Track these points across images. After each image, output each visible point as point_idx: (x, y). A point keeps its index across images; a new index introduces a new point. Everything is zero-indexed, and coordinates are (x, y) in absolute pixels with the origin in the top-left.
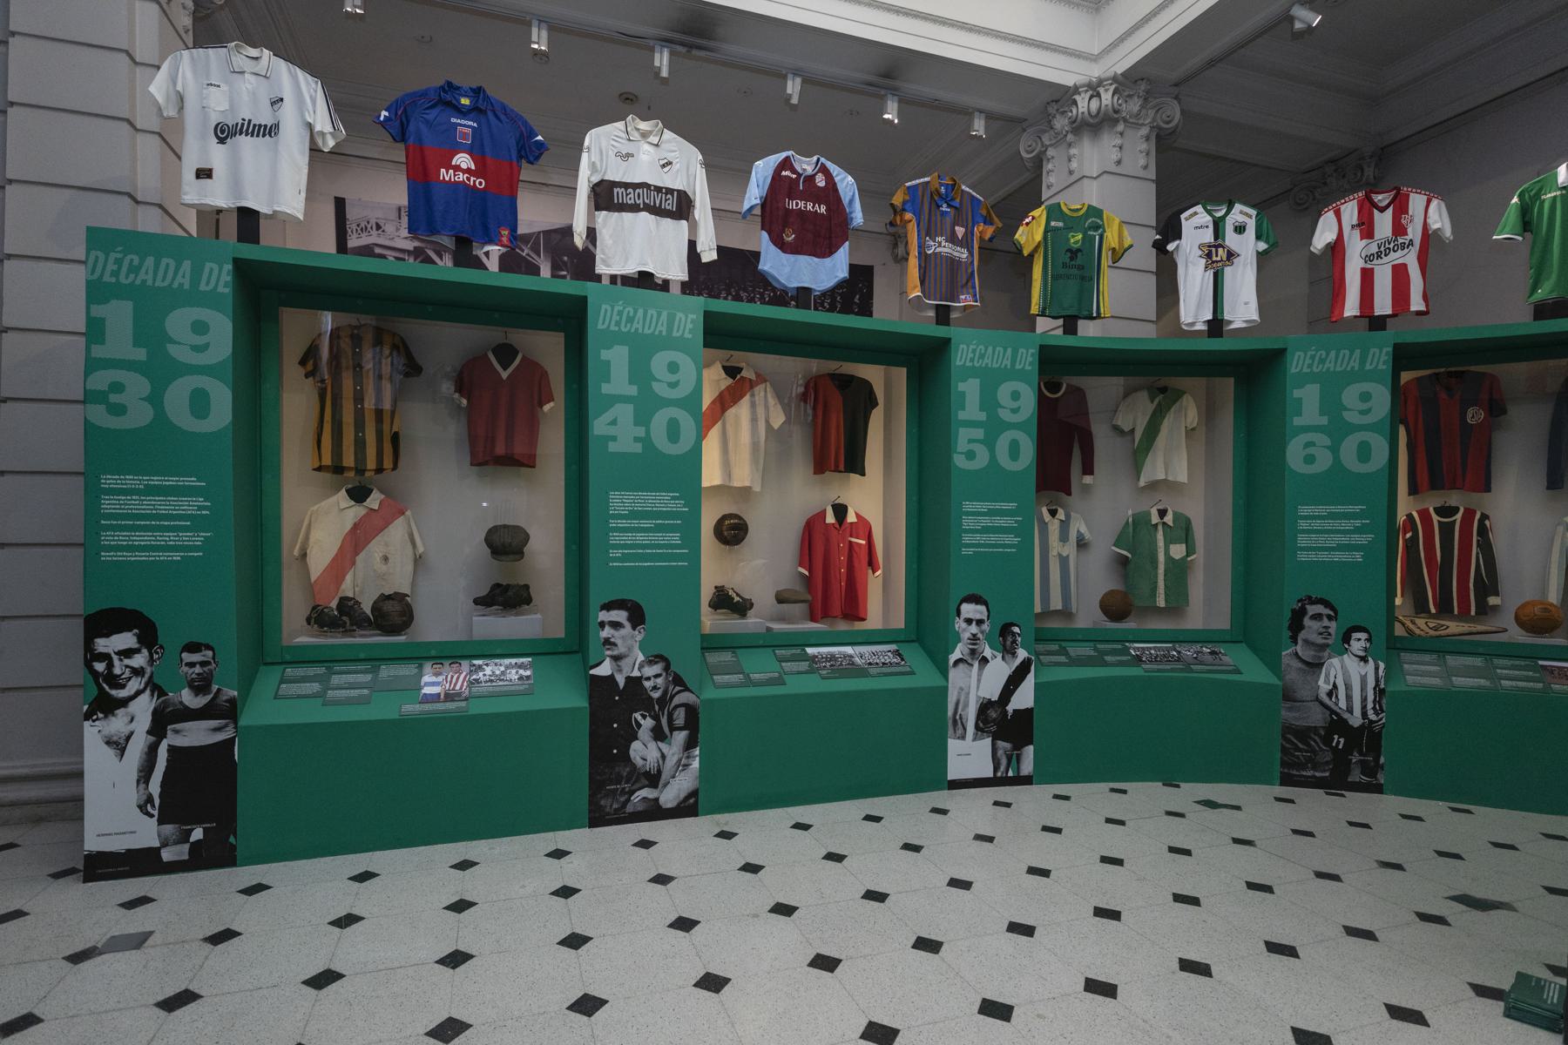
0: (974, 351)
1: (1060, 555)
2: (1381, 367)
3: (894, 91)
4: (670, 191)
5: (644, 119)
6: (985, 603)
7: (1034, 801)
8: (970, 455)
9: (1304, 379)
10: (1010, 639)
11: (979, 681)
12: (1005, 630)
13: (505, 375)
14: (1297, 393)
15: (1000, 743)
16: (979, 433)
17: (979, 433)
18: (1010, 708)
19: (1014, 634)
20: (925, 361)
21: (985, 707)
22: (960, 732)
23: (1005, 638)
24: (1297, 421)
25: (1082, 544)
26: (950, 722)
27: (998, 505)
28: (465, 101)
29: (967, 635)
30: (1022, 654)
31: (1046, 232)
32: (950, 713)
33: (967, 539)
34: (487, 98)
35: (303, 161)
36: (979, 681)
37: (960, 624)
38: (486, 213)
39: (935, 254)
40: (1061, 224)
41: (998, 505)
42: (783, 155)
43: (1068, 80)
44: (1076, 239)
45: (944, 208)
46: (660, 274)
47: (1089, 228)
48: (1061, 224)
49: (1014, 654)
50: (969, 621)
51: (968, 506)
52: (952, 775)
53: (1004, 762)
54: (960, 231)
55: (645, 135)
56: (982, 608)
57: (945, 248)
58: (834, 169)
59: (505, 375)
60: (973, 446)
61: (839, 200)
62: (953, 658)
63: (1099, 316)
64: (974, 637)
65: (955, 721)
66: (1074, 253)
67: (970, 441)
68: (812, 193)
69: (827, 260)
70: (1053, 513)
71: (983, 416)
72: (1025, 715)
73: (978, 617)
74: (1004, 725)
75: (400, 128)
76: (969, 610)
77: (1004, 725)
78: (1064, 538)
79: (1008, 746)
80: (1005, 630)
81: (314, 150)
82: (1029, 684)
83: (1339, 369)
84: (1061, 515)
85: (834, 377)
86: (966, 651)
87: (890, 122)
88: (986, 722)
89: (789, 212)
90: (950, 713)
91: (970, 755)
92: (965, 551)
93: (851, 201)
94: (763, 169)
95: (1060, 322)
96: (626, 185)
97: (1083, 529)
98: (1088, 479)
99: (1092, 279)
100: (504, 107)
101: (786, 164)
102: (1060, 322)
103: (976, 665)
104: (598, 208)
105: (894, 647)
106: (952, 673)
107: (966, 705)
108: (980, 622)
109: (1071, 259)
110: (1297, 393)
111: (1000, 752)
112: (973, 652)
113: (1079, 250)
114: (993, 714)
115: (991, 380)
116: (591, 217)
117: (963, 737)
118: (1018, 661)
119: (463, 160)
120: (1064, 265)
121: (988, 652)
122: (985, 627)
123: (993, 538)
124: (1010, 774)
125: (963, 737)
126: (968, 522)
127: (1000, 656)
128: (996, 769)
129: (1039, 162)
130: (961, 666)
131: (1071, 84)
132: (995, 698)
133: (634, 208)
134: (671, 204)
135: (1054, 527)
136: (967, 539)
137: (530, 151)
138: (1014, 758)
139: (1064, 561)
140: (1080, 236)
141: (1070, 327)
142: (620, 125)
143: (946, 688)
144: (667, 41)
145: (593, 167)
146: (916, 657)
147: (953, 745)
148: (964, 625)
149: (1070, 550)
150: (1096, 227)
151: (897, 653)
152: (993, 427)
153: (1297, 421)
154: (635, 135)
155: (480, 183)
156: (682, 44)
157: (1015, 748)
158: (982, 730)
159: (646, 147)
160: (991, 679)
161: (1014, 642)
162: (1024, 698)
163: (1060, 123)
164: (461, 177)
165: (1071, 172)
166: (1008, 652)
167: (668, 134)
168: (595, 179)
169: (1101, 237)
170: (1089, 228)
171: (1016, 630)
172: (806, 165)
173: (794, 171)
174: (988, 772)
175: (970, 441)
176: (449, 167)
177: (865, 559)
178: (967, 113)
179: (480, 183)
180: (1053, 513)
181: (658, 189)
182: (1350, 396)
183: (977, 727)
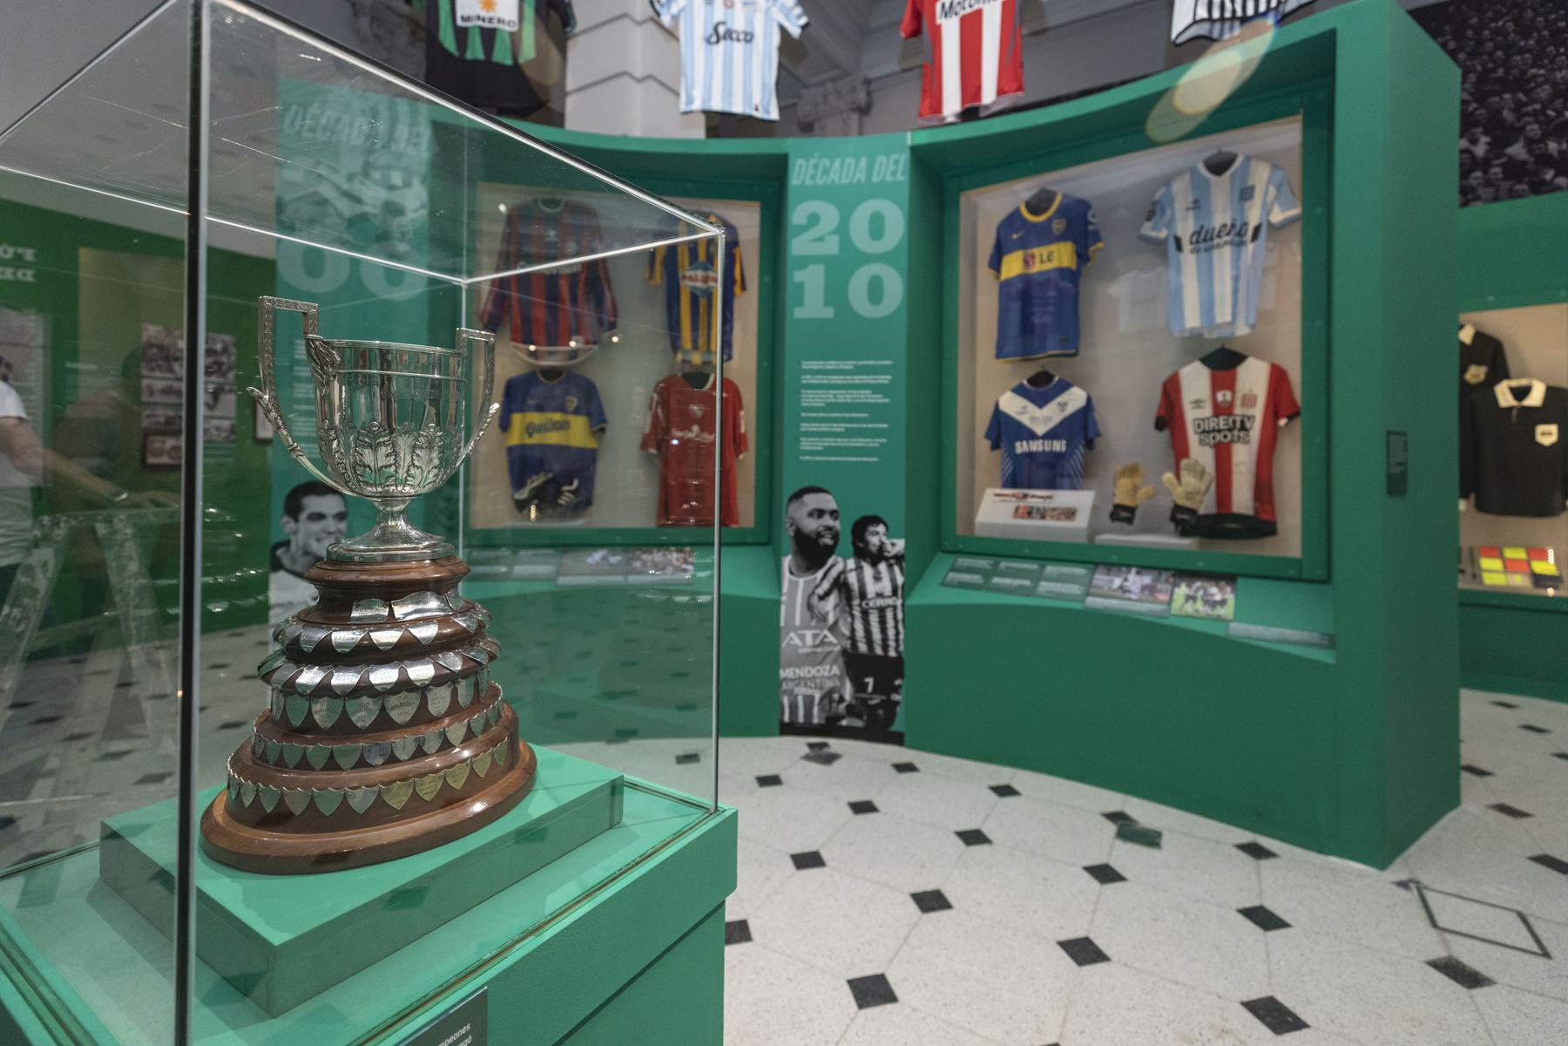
51: (806, 365)
83: (844, 181)
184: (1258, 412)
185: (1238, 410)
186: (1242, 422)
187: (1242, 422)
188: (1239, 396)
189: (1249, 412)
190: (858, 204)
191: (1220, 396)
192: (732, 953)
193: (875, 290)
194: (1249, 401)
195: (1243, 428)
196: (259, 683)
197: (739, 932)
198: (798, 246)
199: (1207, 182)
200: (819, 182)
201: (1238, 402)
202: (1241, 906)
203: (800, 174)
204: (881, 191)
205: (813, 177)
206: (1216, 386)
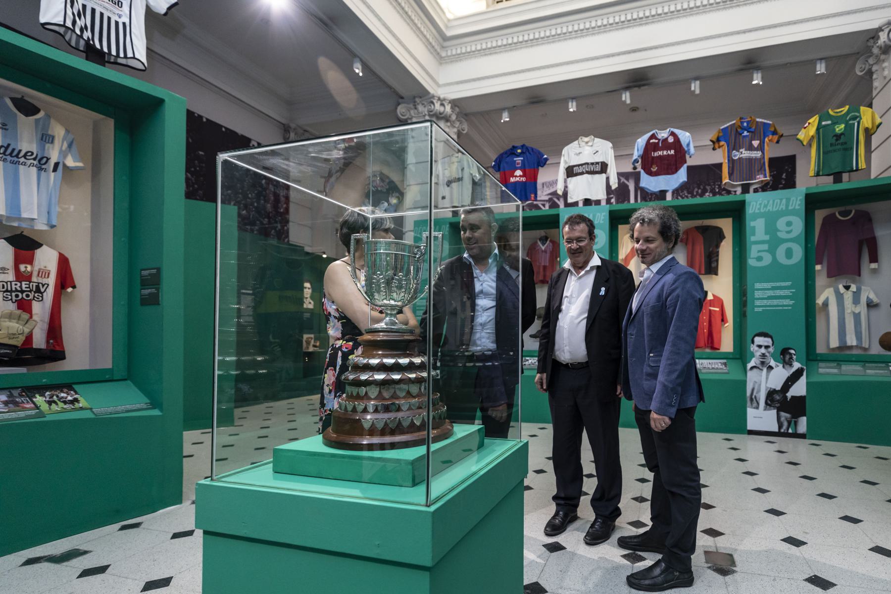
0: (760, 204)
1: (854, 313)
2: (797, 207)
3: (758, 68)
4: (597, 163)
5: (586, 136)
6: (771, 337)
7: (800, 449)
8: (759, 259)
9: (756, 217)
10: (788, 357)
11: (767, 378)
12: (785, 352)
13: (543, 248)
14: (752, 224)
15: (782, 414)
16: (765, 247)
17: (765, 247)
18: (789, 395)
19: (791, 354)
20: (737, 212)
21: (771, 394)
22: (755, 404)
23: (785, 356)
24: (753, 239)
25: (871, 305)
26: (748, 400)
27: (778, 284)
28: (519, 151)
29: (758, 354)
30: (797, 365)
31: (818, 129)
32: (748, 394)
33: (757, 303)
34: (527, 148)
35: (470, 187)
36: (767, 378)
37: (753, 348)
38: (526, 191)
39: (740, 159)
40: (829, 122)
41: (778, 284)
42: (651, 133)
43: (875, 25)
44: (840, 128)
45: (745, 133)
46: (594, 198)
47: (850, 119)
48: (829, 122)
49: (791, 365)
50: (760, 346)
51: (758, 286)
52: (750, 427)
53: (785, 424)
54: (756, 143)
55: (587, 143)
56: (769, 340)
57: (745, 154)
58: (676, 131)
59: (543, 248)
60: (760, 254)
61: (681, 145)
62: (749, 366)
63: (857, 170)
64: (763, 355)
65: (751, 400)
66: (838, 137)
67: (759, 251)
68: (665, 144)
69: (675, 176)
70: (847, 288)
71: (767, 238)
72: (799, 401)
73: (766, 344)
74: (777, 400)
75: (498, 167)
76: (759, 340)
77: (777, 400)
78: (856, 300)
79: (788, 415)
80: (785, 352)
81: (473, 181)
82: (802, 381)
83: (775, 209)
84: (854, 288)
85: (697, 228)
86: (758, 362)
87: (758, 84)
88: (773, 401)
89: (653, 158)
90: (748, 394)
91: (762, 418)
92: (756, 309)
93: (688, 145)
94: (641, 142)
95: (832, 177)
96: (579, 166)
97: (872, 296)
98: (874, 266)
99: (852, 149)
100: (532, 149)
101: (653, 136)
102: (832, 177)
103: (765, 370)
104: (568, 177)
105: (725, 361)
106: (749, 374)
107: (759, 391)
108: (767, 347)
109: (837, 140)
110: (752, 224)
111: (782, 419)
112: (763, 363)
113: (842, 134)
114: (777, 397)
115: (771, 219)
116: (565, 181)
117: (757, 408)
118: (794, 369)
119: (518, 173)
120: (831, 145)
121: (773, 363)
122: (771, 350)
123: (775, 302)
124: (790, 431)
125: (757, 408)
126: (757, 294)
127: (781, 366)
128: (780, 427)
129: (870, 73)
130: (755, 370)
131: (877, 26)
132: (778, 388)
133: (582, 173)
134: (598, 168)
135: (848, 296)
136: (757, 303)
137: (542, 163)
138: (792, 422)
139: (857, 317)
140: (843, 126)
141: (838, 178)
142: (576, 142)
143: (746, 381)
144: (627, 88)
145: (566, 162)
146: (734, 366)
147: (751, 412)
148: (757, 348)
149: (862, 308)
150: (854, 118)
151: (725, 364)
152: (774, 243)
153: (753, 239)
154: (584, 144)
155: (524, 179)
156: (635, 86)
157: (793, 417)
158: (770, 406)
159: (587, 148)
160: (778, 376)
161: (791, 358)
162: (799, 389)
163: (876, 51)
164: (518, 179)
165: (885, 78)
166: (787, 363)
167: (597, 140)
168: (567, 166)
169: (859, 123)
170: (850, 119)
171: (792, 352)
172: (663, 134)
173: (656, 138)
174: (775, 429)
175: (759, 251)
176: (513, 176)
177: (719, 318)
178: (813, 63)
179: (524, 179)
180: (847, 288)
181: (592, 164)
182: (781, 224)
183: (766, 403)
184: (52, 281)
185: (34, 279)
186: (38, 287)
187: (38, 287)
188: (36, 269)
189: (45, 281)
190: (777, 219)
191: (22, 267)
192: (526, 493)
193: (789, 254)
194: (45, 273)
195: (38, 290)
196: (773, 372)
197: (529, 488)
198: (751, 239)
199: (16, 115)
200: (762, 211)
201: (35, 274)
202: (871, 547)
203: (750, 210)
204: (793, 213)
205: (759, 209)
206: (17, 261)
